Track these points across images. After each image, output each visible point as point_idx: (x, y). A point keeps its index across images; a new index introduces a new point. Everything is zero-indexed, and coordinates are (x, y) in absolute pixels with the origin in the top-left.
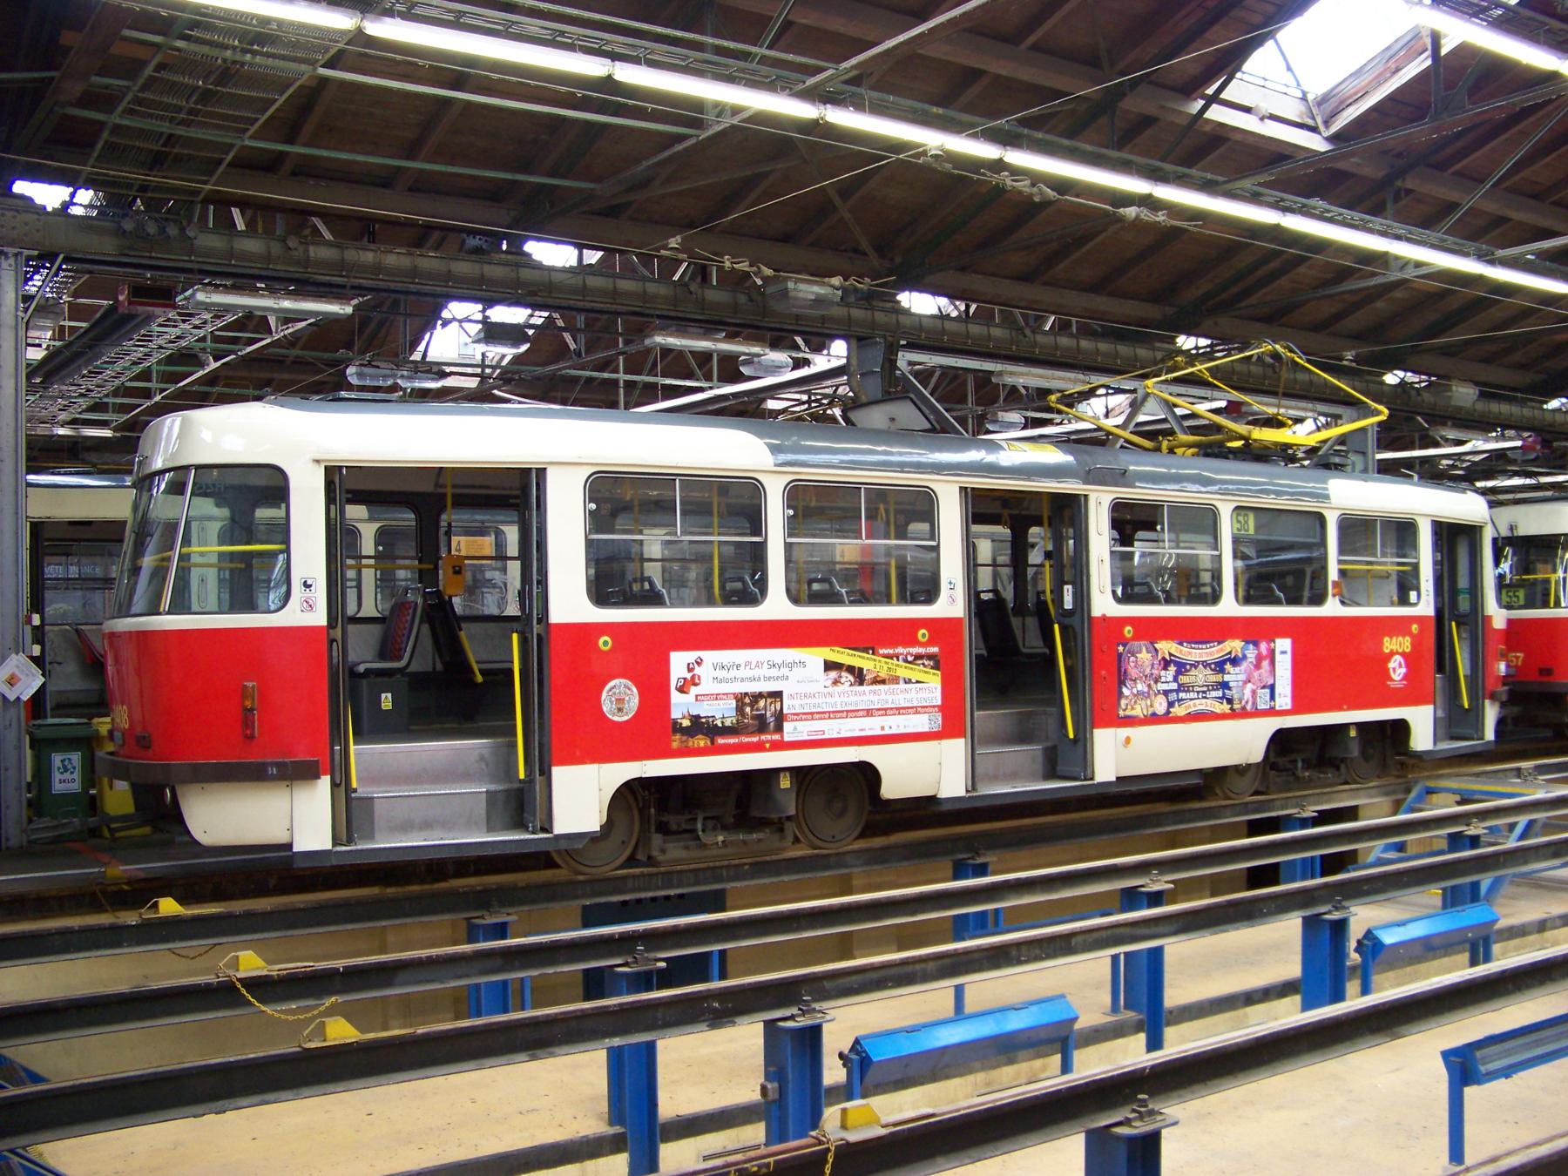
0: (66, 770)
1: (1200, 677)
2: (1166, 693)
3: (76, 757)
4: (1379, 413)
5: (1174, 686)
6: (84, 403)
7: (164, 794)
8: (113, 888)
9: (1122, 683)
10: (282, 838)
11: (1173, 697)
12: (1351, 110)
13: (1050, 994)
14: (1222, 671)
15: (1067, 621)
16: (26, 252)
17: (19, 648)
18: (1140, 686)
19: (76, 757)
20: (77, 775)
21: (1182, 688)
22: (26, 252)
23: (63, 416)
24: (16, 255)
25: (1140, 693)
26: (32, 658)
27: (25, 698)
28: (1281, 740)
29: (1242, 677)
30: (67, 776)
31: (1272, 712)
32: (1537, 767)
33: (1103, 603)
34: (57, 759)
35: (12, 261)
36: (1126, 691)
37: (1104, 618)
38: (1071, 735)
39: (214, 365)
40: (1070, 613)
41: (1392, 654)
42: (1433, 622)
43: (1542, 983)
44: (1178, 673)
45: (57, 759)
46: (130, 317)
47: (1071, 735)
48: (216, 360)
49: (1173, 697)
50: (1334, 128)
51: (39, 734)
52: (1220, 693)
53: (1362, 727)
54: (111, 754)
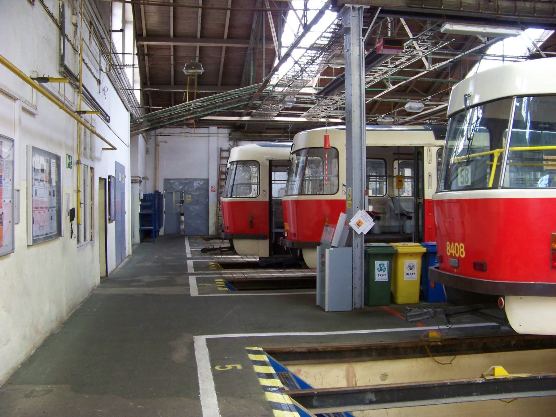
0: (381, 270)
3: (386, 263)
6: (332, 108)
7: (297, 253)
8: (433, 344)
16: (364, 7)
17: (362, 207)
19: (386, 263)
20: (386, 272)
22: (364, 7)
23: (323, 114)
24: (359, 9)
26: (369, 213)
27: (365, 233)
30: (382, 273)
34: (377, 264)
35: (356, 12)
39: (392, 88)
42: (268, 203)
45: (377, 264)
46: (381, 55)
48: (393, 85)
51: (370, 251)
54: (437, 268)
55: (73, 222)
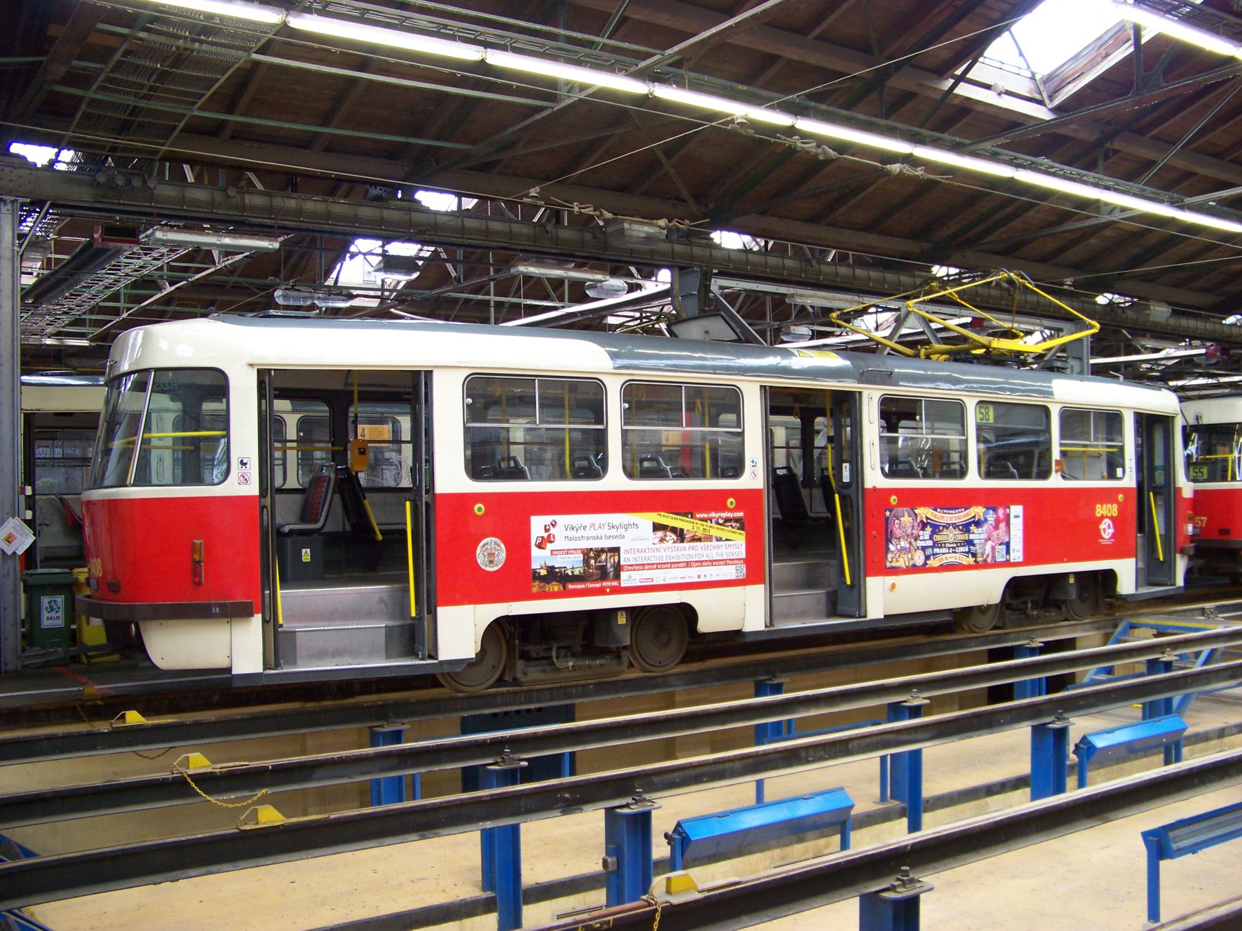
0: (52, 610)
1: (951, 536)
2: (924, 548)
3: (60, 600)
4: (1092, 327)
5: (930, 543)
6: (66, 319)
8: (90, 703)
9: (888, 541)
10: (223, 663)
11: (929, 552)
12: (1070, 87)
13: (831, 787)
14: (968, 531)
15: (845, 492)
16: (21, 200)
17: (15, 513)
18: (903, 543)
19: (60, 600)
20: (61, 614)
21: (936, 545)
22: (21, 200)
23: (50, 330)
24: (13, 202)
25: (903, 549)
26: (26, 521)
27: (20, 552)
28: (1014, 586)
29: (984, 536)
30: (53, 614)
31: (1007, 564)
32: (1217, 607)
33: (874, 477)
34: (45, 601)
35: (9, 206)
36: (892, 547)
37: (875, 489)
38: (849, 582)
39: (169, 289)
40: (848, 485)
41: (1103, 517)
43: (1221, 778)
44: (933, 533)
45: (45, 601)
46: (103, 251)
47: (849, 582)
48: (171, 285)
49: (929, 552)
50: (1057, 102)
51: (31, 581)
52: (966, 549)
53: (1079, 575)
54: (88, 597)
55: (534, 655)
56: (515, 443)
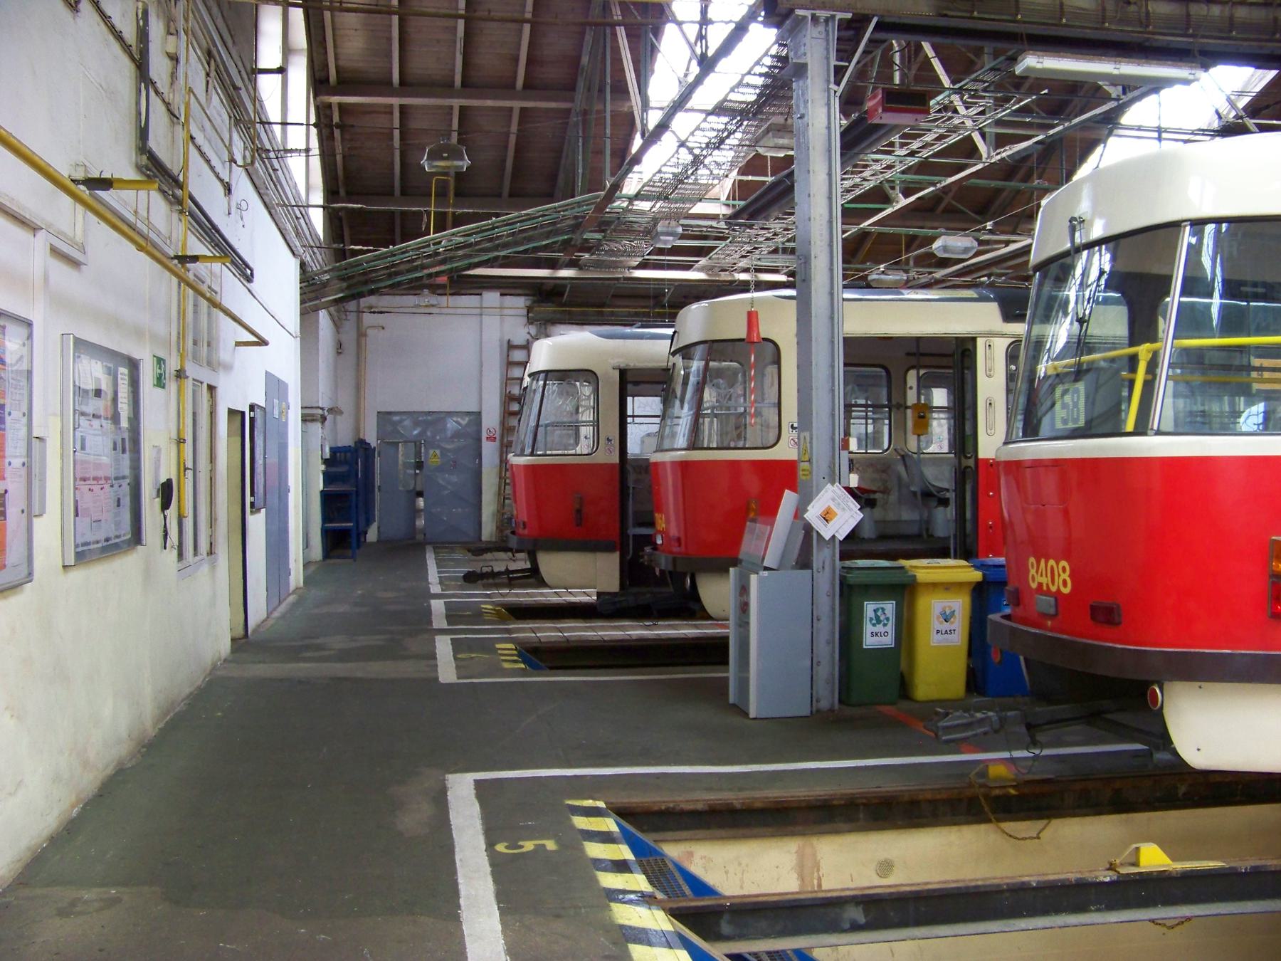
0: (879, 621)
3: (889, 607)
6: (765, 248)
7: (684, 582)
8: (997, 792)
16: (839, 15)
17: (833, 477)
19: (889, 607)
20: (890, 628)
22: (839, 15)
23: (743, 263)
24: (827, 20)
26: (849, 490)
27: (841, 536)
30: (879, 628)
34: (869, 608)
35: (821, 28)
39: (903, 202)
42: (618, 469)
45: (869, 608)
46: (878, 127)
48: (906, 195)
51: (852, 578)
54: (1007, 617)
55: (167, 512)
56: (919, 441)
